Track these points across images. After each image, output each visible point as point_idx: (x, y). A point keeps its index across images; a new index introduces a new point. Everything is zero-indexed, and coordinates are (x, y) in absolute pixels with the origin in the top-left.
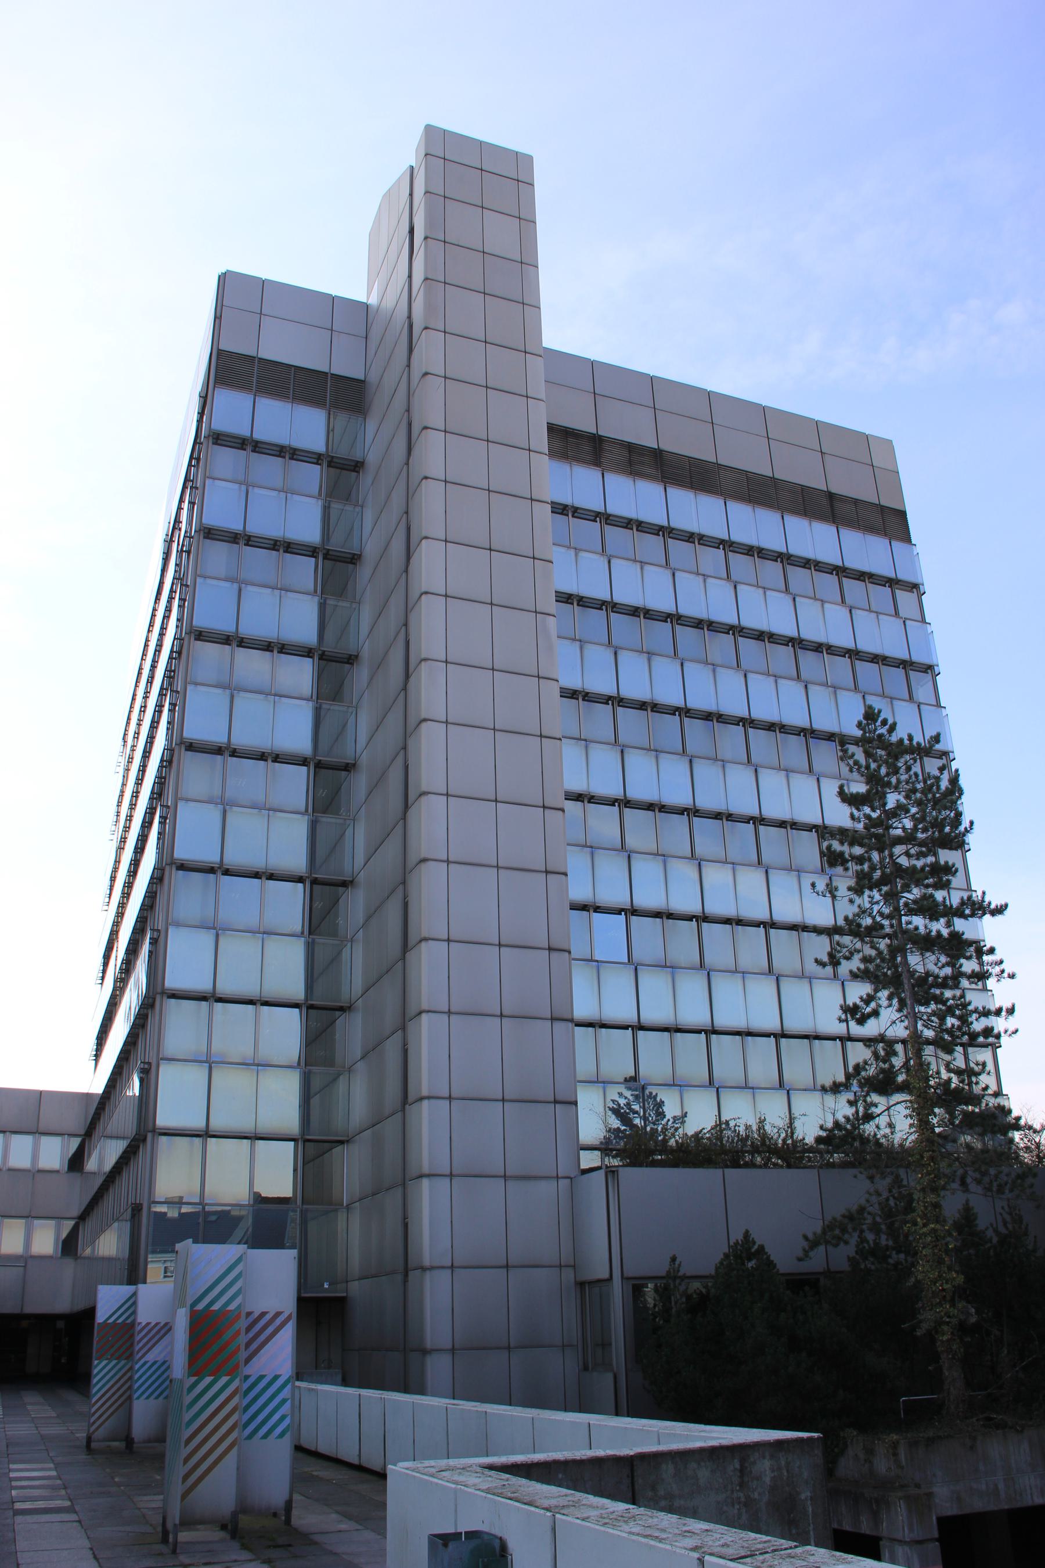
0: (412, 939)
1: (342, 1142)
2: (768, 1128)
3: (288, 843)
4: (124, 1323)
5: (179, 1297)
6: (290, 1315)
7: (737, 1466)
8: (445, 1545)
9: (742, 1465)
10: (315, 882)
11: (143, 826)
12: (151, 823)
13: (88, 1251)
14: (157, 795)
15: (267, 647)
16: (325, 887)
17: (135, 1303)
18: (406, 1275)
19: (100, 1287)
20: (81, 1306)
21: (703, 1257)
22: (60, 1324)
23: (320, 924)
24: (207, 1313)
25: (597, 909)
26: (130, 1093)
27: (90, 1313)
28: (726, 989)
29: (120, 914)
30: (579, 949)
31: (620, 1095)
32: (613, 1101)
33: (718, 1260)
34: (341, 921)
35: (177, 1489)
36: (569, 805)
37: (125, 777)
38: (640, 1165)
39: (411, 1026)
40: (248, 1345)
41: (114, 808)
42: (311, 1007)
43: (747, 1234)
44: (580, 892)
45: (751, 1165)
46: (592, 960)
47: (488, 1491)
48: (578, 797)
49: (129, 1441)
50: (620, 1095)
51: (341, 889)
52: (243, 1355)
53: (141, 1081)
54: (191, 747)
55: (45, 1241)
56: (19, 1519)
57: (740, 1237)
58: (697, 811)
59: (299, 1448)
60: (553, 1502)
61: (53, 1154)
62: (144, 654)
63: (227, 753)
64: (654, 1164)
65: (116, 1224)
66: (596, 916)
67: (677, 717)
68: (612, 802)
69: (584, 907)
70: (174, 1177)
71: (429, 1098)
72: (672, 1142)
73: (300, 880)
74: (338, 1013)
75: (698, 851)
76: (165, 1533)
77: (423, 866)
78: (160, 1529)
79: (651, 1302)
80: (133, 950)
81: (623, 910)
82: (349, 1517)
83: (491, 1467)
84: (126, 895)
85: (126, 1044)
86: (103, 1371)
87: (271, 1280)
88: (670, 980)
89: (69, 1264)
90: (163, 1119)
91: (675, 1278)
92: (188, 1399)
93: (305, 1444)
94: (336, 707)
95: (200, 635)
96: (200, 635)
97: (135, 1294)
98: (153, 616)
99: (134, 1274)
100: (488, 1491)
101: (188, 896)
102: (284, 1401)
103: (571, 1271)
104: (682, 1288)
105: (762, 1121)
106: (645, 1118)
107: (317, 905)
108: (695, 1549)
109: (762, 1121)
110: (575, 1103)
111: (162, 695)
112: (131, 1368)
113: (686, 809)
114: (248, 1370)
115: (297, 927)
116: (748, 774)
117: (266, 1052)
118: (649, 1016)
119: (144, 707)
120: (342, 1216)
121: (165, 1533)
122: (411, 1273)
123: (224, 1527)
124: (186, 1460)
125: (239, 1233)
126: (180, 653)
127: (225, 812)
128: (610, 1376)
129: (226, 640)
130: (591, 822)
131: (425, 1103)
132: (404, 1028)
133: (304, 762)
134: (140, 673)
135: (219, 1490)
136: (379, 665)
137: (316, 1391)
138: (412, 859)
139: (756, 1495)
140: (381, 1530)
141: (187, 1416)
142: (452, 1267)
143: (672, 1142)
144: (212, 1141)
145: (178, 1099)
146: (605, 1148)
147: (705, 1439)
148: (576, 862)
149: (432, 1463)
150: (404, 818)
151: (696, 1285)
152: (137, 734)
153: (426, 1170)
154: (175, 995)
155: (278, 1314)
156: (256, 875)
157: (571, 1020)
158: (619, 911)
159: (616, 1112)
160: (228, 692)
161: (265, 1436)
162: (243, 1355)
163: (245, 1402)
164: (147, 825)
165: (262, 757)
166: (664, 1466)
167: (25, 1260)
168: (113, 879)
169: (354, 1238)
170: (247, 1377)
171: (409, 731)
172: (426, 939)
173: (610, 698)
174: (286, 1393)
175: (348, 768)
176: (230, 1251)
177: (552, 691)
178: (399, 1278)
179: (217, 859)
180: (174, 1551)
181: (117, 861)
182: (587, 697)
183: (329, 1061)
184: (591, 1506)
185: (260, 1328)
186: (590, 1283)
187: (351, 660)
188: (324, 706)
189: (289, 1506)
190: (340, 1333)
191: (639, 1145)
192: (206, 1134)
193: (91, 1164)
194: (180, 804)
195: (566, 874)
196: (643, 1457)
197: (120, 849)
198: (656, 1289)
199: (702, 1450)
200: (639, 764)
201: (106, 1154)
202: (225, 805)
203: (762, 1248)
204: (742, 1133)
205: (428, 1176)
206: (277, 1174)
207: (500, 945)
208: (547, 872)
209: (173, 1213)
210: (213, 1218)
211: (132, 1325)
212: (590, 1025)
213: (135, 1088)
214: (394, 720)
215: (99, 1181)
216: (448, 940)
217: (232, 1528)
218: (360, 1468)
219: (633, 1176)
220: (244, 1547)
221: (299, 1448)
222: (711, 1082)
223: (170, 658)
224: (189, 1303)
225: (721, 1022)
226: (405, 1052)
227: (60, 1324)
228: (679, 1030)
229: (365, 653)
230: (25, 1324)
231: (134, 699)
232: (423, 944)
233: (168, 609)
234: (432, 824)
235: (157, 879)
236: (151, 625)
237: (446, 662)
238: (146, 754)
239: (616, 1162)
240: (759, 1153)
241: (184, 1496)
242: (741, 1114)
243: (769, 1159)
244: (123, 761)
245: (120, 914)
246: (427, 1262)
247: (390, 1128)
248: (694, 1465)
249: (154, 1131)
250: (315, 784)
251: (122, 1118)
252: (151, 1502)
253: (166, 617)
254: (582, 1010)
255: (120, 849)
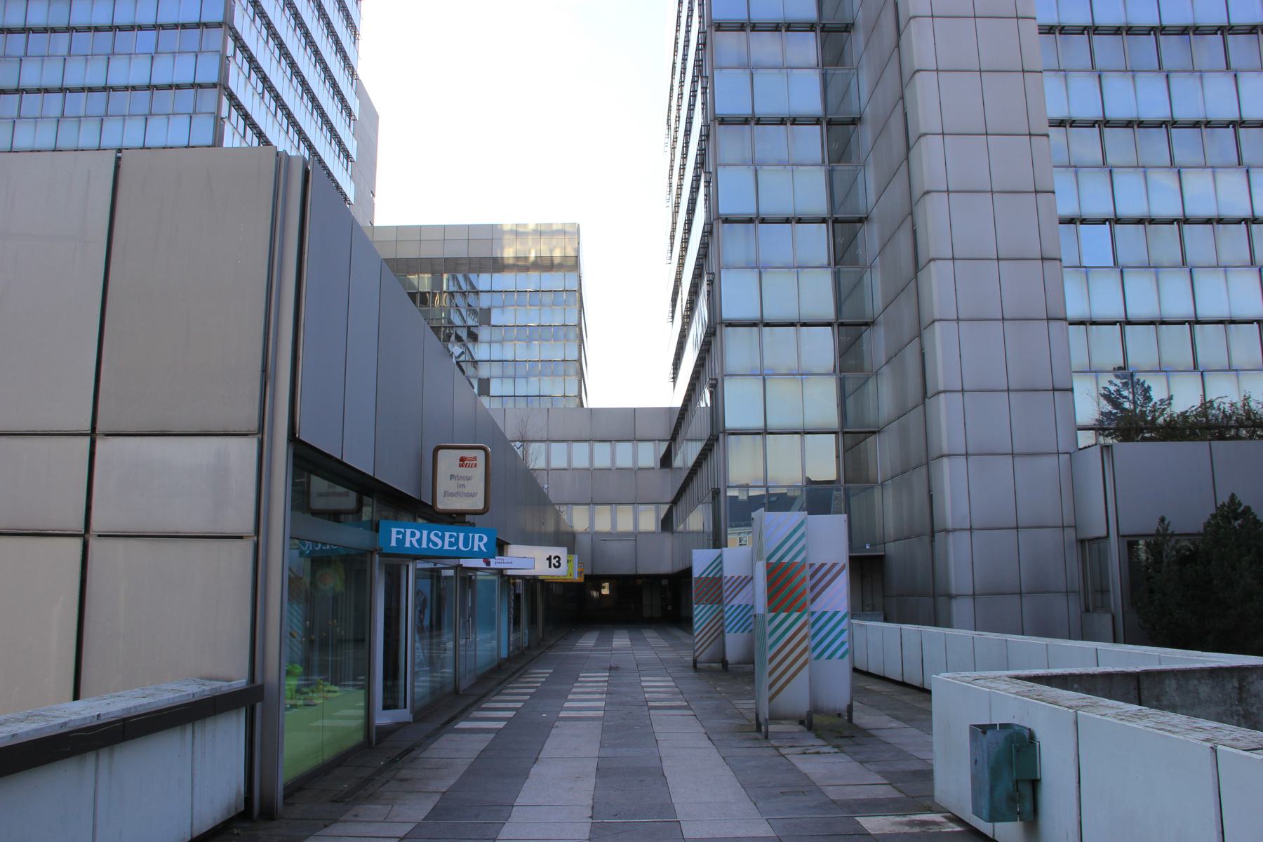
0: (922, 262)
1: (874, 433)
2: (1253, 405)
3: (809, 190)
4: (714, 578)
5: (756, 554)
6: (843, 567)
7: (1236, 684)
8: (984, 733)
9: (1240, 684)
10: (836, 221)
11: (691, 192)
12: (698, 188)
13: (681, 527)
14: (701, 164)
15: (776, 28)
16: (844, 226)
17: (721, 562)
18: (933, 536)
19: (694, 551)
20: (679, 567)
21: (1191, 516)
22: (665, 582)
23: (843, 256)
24: (780, 564)
25: (1083, 221)
26: (703, 405)
27: (688, 572)
28: (1209, 283)
29: (681, 265)
30: (1069, 257)
31: (1110, 382)
32: (1105, 388)
33: (1205, 520)
34: (860, 251)
35: (765, 694)
36: (1056, 133)
37: (673, 155)
38: (1132, 440)
39: (926, 333)
40: (812, 588)
41: (667, 181)
42: (841, 324)
43: (1233, 497)
44: (1067, 208)
45: (1237, 437)
46: (1080, 267)
47: (1017, 693)
48: (1061, 123)
49: (724, 663)
50: (1110, 382)
51: (859, 225)
52: (809, 596)
53: (711, 393)
54: (723, 121)
55: (649, 520)
56: (652, 712)
57: (1227, 500)
58: (1175, 122)
59: (855, 670)
60: (1074, 703)
61: (649, 455)
62: (676, 51)
63: (753, 123)
64: (1144, 439)
65: (700, 506)
66: (1082, 228)
67: (1152, 37)
68: (1093, 124)
69: (1071, 221)
70: (743, 467)
71: (945, 392)
72: (1161, 420)
73: (824, 221)
74: (864, 328)
75: (1177, 160)
76: (759, 725)
77: (927, 197)
78: (754, 722)
79: (1143, 556)
80: (694, 292)
81: (1107, 220)
82: (897, 718)
83: (1017, 678)
84: (684, 249)
85: (696, 366)
86: (701, 613)
87: (828, 539)
88: (1154, 282)
89: (667, 535)
90: (731, 422)
91: (1165, 535)
92: (770, 629)
93: (858, 667)
94: (840, 71)
95: (719, 27)
96: (719, 27)
97: (720, 555)
98: (679, 17)
99: (718, 541)
100: (1017, 693)
101: (734, 242)
102: (842, 631)
103: (1072, 531)
104: (1171, 544)
105: (1246, 399)
106: (1134, 403)
107: (840, 240)
108: (1207, 740)
109: (1246, 399)
110: (1072, 390)
111: (694, 82)
112: (722, 611)
113: (1164, 122)
114: (813, 608)
115: (824, 260)
116: (1228, 79)
117: (807, 365)
118: (1135, 312)
119: (681, 95)
120: (877, 492)
121: (759, 725)
122: (937, 535)
123: (801, 723)
124: (771, 674)
125: (797, 504)
126: (704, 44)
127: (756, 171)
128: (1109, 617)
129: (741, 27)
130: (1074, 147)
131: (942, 396)
132: (920, 335)
133: (817, 121)
134: (674, 67)
135: (797, 696)
136: (874, 27)
137: (865, 626)
138: (917, 193)
139: (1255, 710)
140: (928, 730)
141: (770, 642)
142: (971, 529)
143: (1161, 420)
144: (770, 437)
145: (741, 406)
146: (1099, 428)
147: (1204, 662)
148: (1062, 182)
149: (968, 674)
150: (907, 158)
151: (1185, 543)
152: (678, 117)
153: (945, 451)
154: (730, 325)
155: (834, 565)
156: (788, 221)
157: (1065, 319)
158: (1103, 222)
159: (1108, 397)
160: (748, 71)
161: (830, 657)
162: (809, 596)
163: (813, 632)
164: (695, 190)
165: (782, 122)
166: (1167, 682)
167: (635, 536)
168: (672, 237)
169: (889, 510)
170: (813, 613)
171: (904, 83)
172: (934, 260)
173: (1085, 28)
174: (844, 625)
175: (855, 122)
176: (794, 517)
177: (1030, 29)
178: (927, 539)
179: (754, 211)
180: (766, 738)
181: (674, 223)
182: (1063, 30)
183: (859, 368)
184: (1107, 706)
185: (821, 576)
186: (1089, 540)
187: (848, 28)
188: (830, 72)
189: (850, 709)
190: (879, 581)
191: (1129, 424)
192: (765, 432)
193: (677, 462)
194: (720, 170)
195: (1053, 192)
196: (1148, 674)
197: (676, 212)
198: (1147, 545)
199: (1202, 670)
200: (1117, 86)
201: (687, 454)
202: (756, 165)
203: (1248, 509)
204: (1228, 411)
205: (948, 455)
206: (823, 462)
207: (998, 259)
208: (1036, 192)
209: (743, 496)
210: (774, 499)
211: (720, 579)
212: (1082, 323)
213: (706, 400)
214: (891, 74)
215: (685, 474)
216: (953, 259)
217: (808, 723)
218: (903, 684)
219: (1124, 450)
220: (818, 736)
221: (855, 670)
222: (1195, 367)
223: (697, 50)
224: (766, 556)
225: (1204, 313)
226: (923, 355)
227: (665, 582)
228: (1163, 323)
229: (860, 21)
230: (639, 582)
231: (672, 89)
232: (932, 264)
233: (691, 10)
234: (932, 161)
235: (708, 232)
236: (678, 25)
237: (932, 16)
238: (688, 133)
239: (1109, 441)
240: (1245, 427)
241: (771, 699)
242: (1226, 394)
243: (1254, 432)
244: (669, 141)
245: (681, 265)
246: (950, 525)
247: (915, 417)
248: (1196, 682)
249: (724, 432)
250: (828, 139)
251: (698, 426)
252: (746, 705)
253: (690, 16)
254: (1073, 311)
255: (676, 212)
